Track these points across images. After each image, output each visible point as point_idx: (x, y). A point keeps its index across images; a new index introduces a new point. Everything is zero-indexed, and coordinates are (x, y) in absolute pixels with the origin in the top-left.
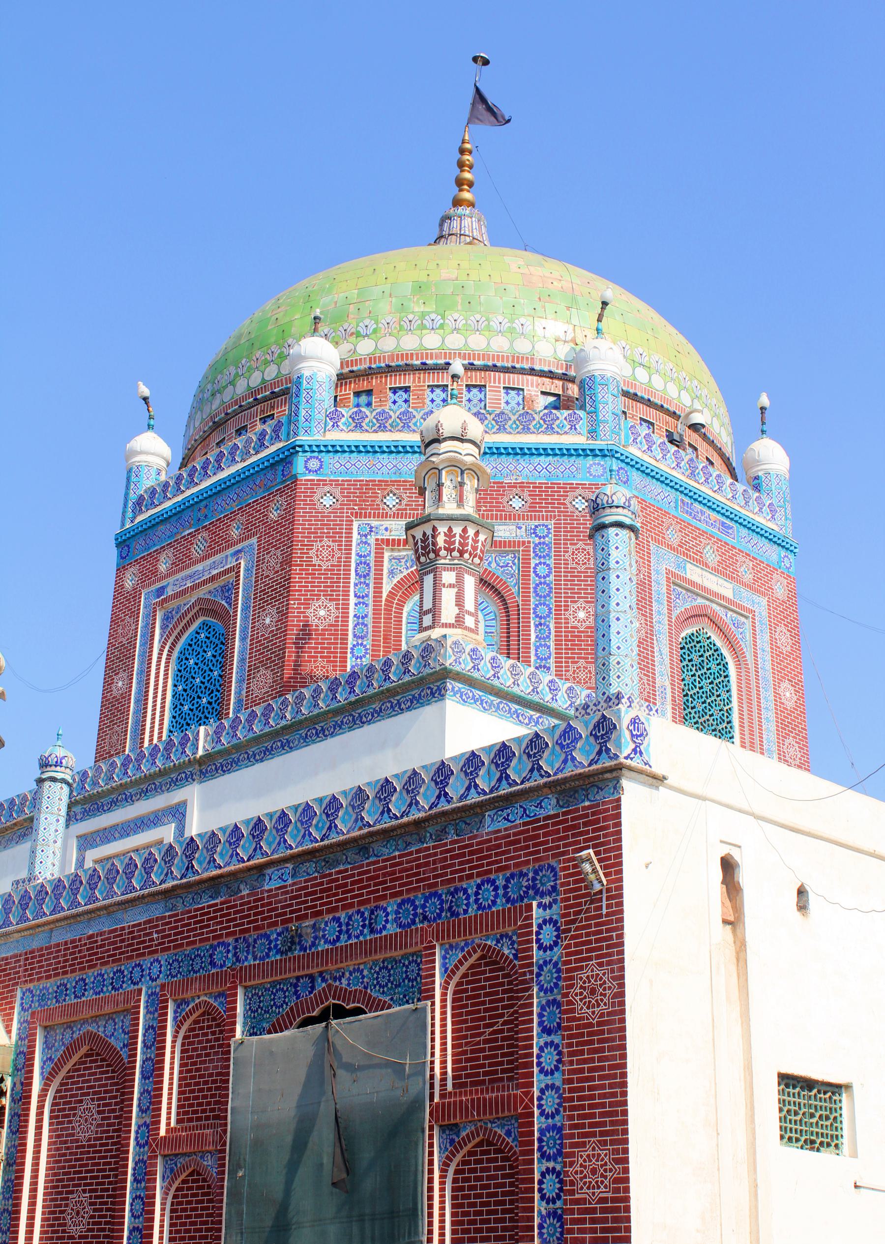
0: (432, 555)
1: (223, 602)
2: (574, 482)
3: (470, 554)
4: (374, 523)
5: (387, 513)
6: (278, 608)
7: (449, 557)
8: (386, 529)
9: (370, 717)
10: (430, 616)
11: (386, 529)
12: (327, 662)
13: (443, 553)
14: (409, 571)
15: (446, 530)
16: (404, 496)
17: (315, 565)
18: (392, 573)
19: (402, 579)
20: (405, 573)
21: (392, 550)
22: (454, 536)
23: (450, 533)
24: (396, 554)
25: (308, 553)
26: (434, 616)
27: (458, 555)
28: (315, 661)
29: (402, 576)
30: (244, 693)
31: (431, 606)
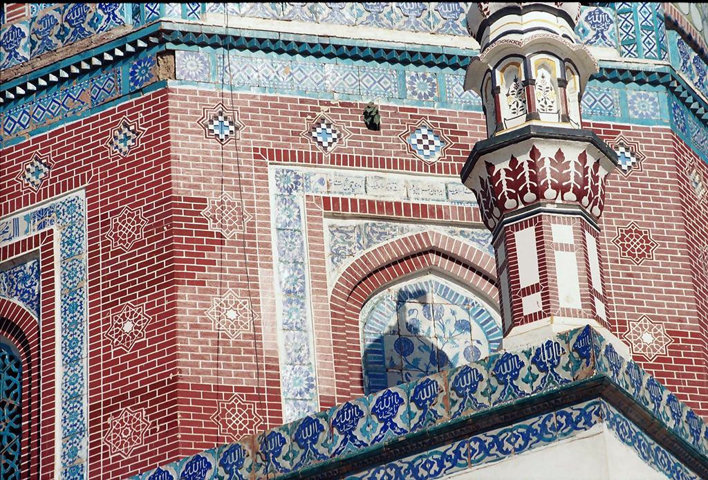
0: (530, 197)
1: (15, 300)
2: (612, 123)
3: (590, 199)
4: (302, 170)
5: (320, 155)
6: (148, 306)
7: (559, 201)
8: (321, 181)
9: (435, 468)
10: (537, 296)
11: (321, 181)
12: (249, 397)
13: (550, 193)
14: (364, 253)
15: (506, 165)
16: (344, 128)
17: (211, 234)
18: (336, 254)
19: (353, 265)
20: (358, 257)
21: (334, 216)
22: (567, 165)
23: (515, 168)
24: (339, 222)
25: (198, 213)
26: (545, 297)
27: (574, 197)
28: (227, 396)
29: (352, 260)
30: (84, 453)
31: (537, 280)
